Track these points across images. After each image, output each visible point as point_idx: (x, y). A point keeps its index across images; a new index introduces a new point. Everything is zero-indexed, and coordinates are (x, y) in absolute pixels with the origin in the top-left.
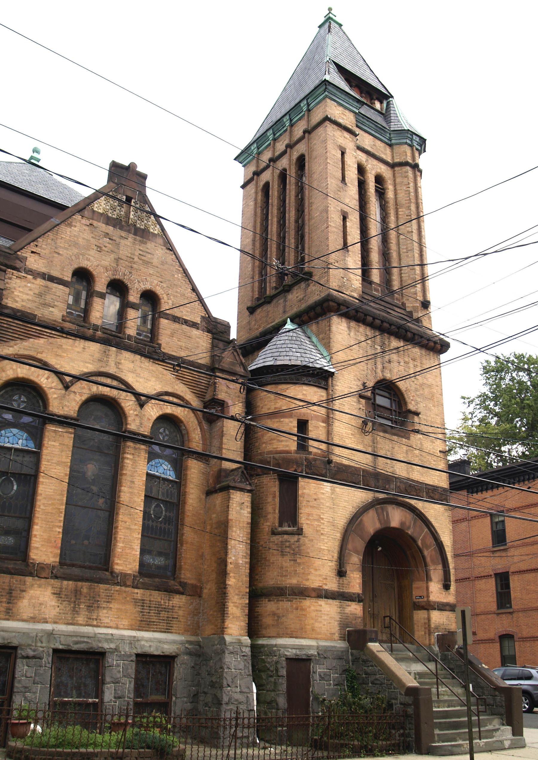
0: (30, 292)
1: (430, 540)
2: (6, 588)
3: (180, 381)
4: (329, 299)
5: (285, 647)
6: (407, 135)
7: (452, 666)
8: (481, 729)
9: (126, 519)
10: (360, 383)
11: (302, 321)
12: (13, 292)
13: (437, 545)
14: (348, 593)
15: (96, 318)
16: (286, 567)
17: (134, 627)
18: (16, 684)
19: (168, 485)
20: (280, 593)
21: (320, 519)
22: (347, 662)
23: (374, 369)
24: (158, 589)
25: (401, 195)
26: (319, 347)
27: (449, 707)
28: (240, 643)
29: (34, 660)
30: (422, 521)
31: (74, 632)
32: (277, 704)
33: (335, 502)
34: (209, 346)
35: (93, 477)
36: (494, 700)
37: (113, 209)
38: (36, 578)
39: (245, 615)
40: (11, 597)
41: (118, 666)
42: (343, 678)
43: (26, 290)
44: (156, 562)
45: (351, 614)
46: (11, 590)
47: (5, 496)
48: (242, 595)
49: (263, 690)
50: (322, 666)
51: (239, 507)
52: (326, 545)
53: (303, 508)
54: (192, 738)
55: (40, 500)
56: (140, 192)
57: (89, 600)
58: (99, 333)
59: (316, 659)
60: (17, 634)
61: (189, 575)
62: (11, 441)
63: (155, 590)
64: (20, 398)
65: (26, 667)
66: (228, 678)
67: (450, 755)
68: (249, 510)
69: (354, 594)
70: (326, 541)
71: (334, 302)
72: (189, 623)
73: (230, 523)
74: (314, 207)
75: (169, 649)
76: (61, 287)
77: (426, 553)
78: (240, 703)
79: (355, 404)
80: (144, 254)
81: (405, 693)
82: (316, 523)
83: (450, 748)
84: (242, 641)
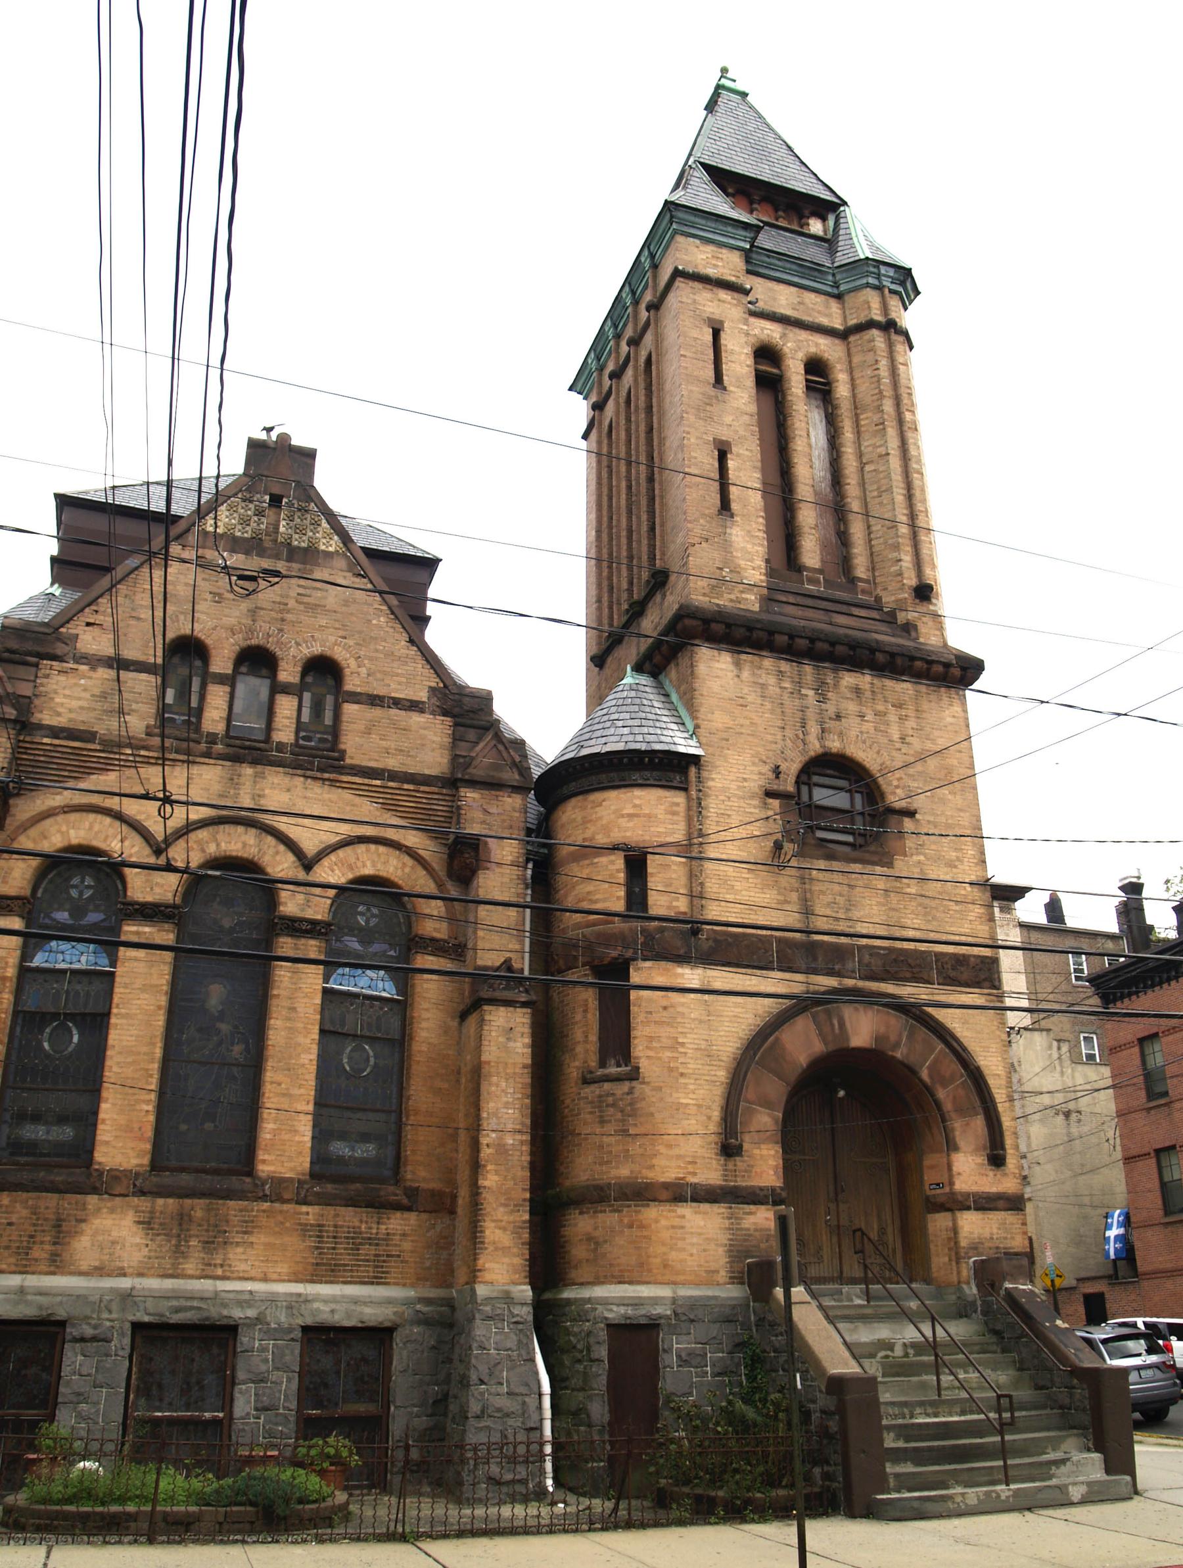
0: (83, 694)
1: (952, 1066)
2: (52, 1217)
3: (390, 813)
4: (685, 613)
5: (605, 1302)
6: (866, 269)
7: (999, 1327)
8: (1009, 1462)
9: (279, 1077)
10: (766, 769)
11: (655, 666)
12: (52, 699)
13: (968, 1076)
14: (747, 1188)
15: (213, 720)
16: (608, 1145)
17: (300, 1276)
18: (62, 1389)
19: (381, 1009)
20: (600, 1196)
21: (675, 1045)
22: (746, 1326)
23: (801, 736)
24: (351, 1202)
25: (864, 388)
26: (679, 709)
27: (963, 1413)
28: (508, 1298)
29: (95, 1344)
30: (929, 1029)
31: (173, 1290)
32: (588, 1416)
33: (711, 1009)
34: (447, 740)
35: (220, 1008)
36: (1071, 1395)
37: (245, 522)
38: (106, 1196)
39: (523, 1244)
40: (59, 1232)
41: (264, 1349)
42: (736, 1360)
43: (78, 692)
44: (358, 1154)
45: (756, 1230)
46: (59, 1220)
47: (57, 1056)
48: (515, 1206)
49: (566, 1388)
50: (685, 1338)
51: (507, 1037)
52: (691, 1096)
53: (640, 1027)
54: (430, 1484)
55: (111, 1057)
56: (298, 483)
57: (207, 1231)
58: (219, 747)
59: (670, 1325)
60: (65, 1299)
61: (422, 1173)
62: (68, 958)
63: (347, 1206)
64: (83, 881)
65: (80, 1358)
66: (479, 1368)
67: (915, 1519)
68: (527, 1040)
69: (761, 1189)
70: (692, 1087)
71: (695, 618)
72: (428, 1264)
73: (484, 1071)
74: (667, 444)
75: (375, 1314)
76: (144, 676)
77: (941, 1094)
78: (507, 1415)
79: (757, 811)
80: (308, 592)
81: (827, 1387)
82: (668, 1054)
83: (916, 1504)
84: (513, 1295)
